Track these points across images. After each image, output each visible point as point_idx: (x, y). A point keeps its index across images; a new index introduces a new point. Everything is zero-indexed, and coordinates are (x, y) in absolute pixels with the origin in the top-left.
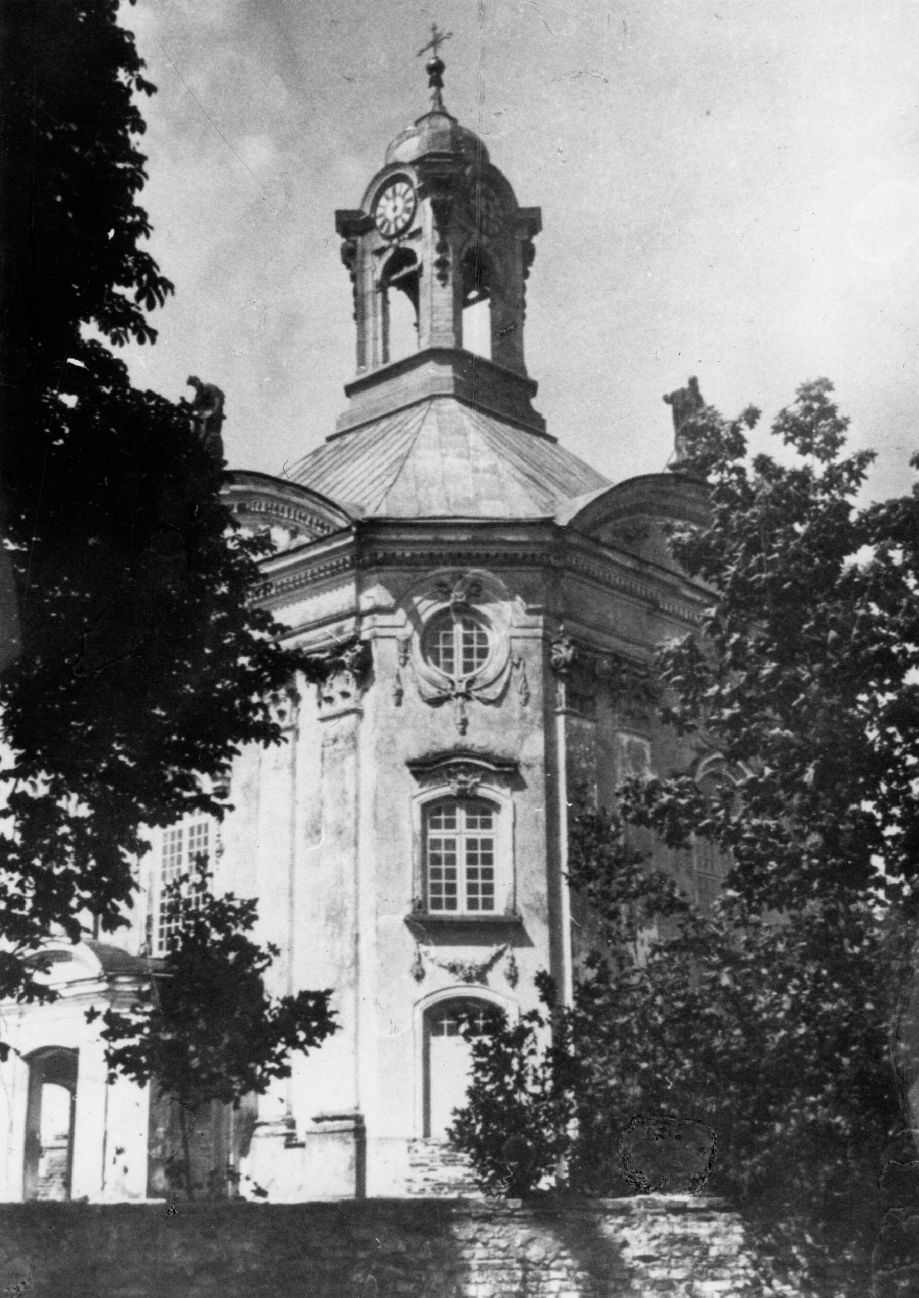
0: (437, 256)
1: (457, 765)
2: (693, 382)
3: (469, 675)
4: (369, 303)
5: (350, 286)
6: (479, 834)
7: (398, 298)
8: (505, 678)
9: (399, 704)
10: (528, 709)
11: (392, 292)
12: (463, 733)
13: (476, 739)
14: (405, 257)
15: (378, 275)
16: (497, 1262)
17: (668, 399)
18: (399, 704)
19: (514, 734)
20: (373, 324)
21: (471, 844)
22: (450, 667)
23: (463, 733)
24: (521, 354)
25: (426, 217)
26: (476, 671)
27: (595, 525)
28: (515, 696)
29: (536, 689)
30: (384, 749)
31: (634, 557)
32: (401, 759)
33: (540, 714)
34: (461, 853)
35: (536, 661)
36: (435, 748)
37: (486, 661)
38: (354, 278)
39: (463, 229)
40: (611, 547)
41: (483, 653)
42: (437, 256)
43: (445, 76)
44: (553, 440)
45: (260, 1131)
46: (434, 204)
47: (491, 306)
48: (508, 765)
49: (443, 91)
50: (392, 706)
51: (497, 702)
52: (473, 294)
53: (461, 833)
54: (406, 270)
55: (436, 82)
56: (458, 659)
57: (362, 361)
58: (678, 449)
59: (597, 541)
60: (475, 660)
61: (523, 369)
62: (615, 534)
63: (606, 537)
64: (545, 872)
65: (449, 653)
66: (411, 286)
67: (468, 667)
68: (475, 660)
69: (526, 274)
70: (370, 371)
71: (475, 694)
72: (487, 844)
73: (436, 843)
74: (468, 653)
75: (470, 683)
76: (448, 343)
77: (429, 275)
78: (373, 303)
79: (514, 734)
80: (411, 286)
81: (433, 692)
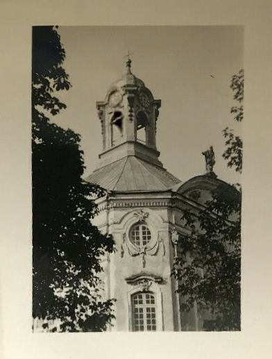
0: (129, 113)
1: (142, 279)
2: (211, 148)
3: (145, 246)
4: (107, 129)
5: (101, 124)
6: (150, 306)
7: (115, 128)
8: (157, 247)
9: (122, 257)
10: (165, 258)
11: (114, 126)
12: (144, 267)
13: (149, 269)
14: (118, 114)
15: (110, 121)
16: (204, 209)
17: (203, 154)
18: (122, 257)
19: (159, 267)
20: (108, 135)
21: (148, 309)
22: (139, 244)
23: (144, 267)
24: (155, 144)
25: (125, 103)
26: (148, 244)
27: (186, 192)
28: (161, 251)
29: (167, 251)
30: (118, 272)
31: (196, 203)
32: (123, 278)
33: (169, 260)
34: (145, 313)
35: (167, 240)
36: (134, 274)
37: (150, 241)
38: (102, 122)
39: (137, 106)
40: (189, 199)
41: (149, 238)
42: (129, 113)
43: (131, 64)
44: (165, 170)
45: (175, 188)
46: (128, 98)
47: (145, 129)
48: (159, 278)
49: (131, 68)
50: (120, 257)
51: (155, 254)
52: (140, 126)
53: (145, 306)
54: (119, 118)
55: (129, 66)
56: (141, 241)
57: (104, 148)
58: (207, 169)
59: (185, 198)
60: (147, 240)
61: (156, 148)
62: (190, 195)
63: (187, 196)
64: (172, 321)
65: (138, 238)
66: (119, 124)
67: (145, 243)
68: (147, 240)
69: (156, 119)
70: (107, 149)
71: (147, 253)
72: (153, 310)
73: (141, 297)
74: (144, 238)
75: (146, 248)
76: (134, 140)
77: (125, 122)
78: (108, 128)
79: (159, 267)
80: (119, 124)
81: (134, 252)
